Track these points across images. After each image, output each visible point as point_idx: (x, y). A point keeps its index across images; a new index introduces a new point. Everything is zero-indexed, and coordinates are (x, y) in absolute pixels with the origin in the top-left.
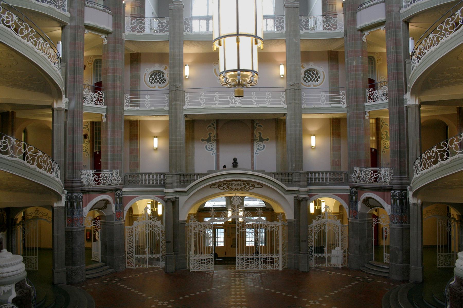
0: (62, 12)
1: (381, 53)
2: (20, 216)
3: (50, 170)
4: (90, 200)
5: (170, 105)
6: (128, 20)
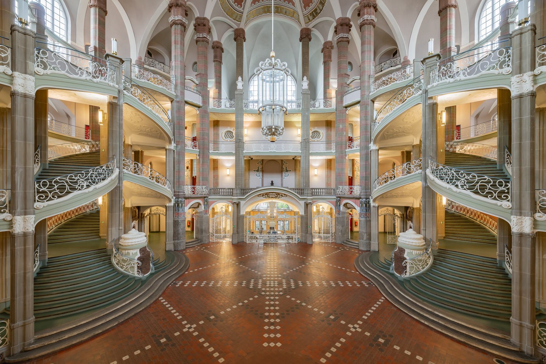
0: (171, 92)
1: (357, 122)
2: (147, 212)
3: (164, 184)
5: (236, 150)
6: (211, 101)
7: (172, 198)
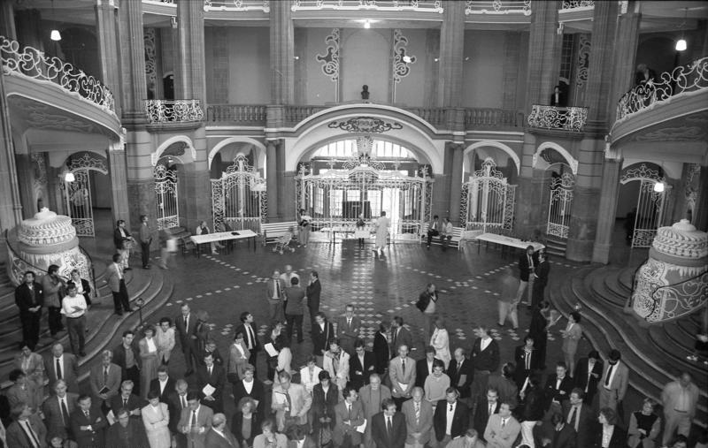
3: (98, 99)
7: (121, 132)
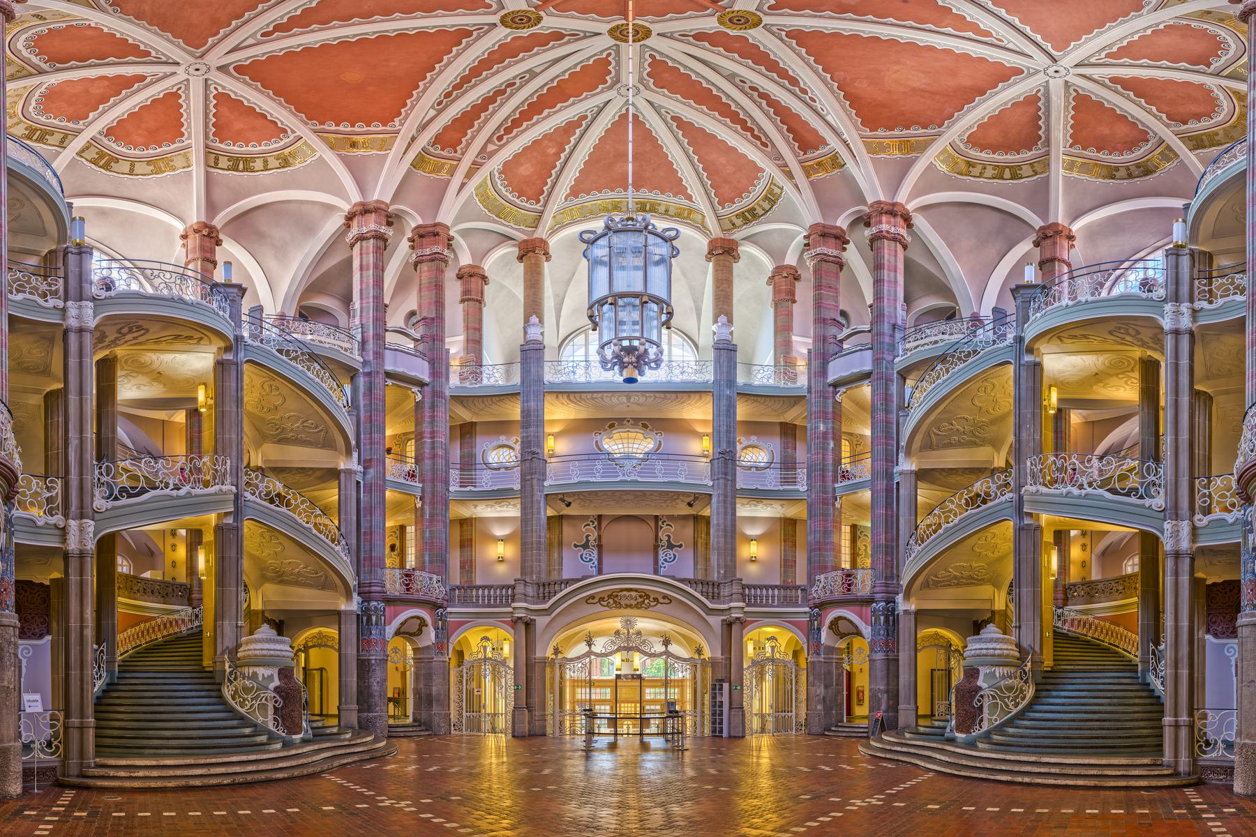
1: (862, 436)
4: (395, 616)
